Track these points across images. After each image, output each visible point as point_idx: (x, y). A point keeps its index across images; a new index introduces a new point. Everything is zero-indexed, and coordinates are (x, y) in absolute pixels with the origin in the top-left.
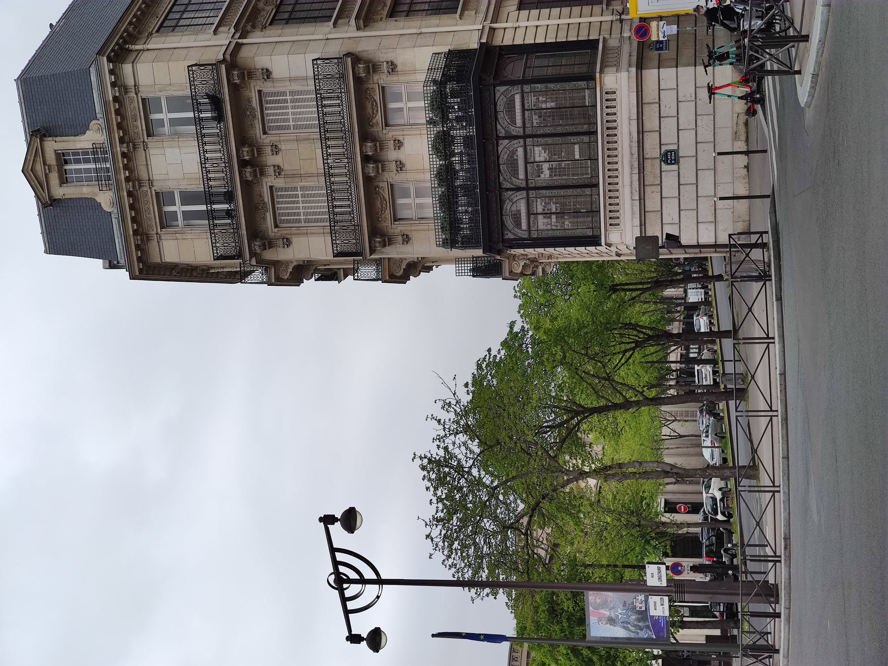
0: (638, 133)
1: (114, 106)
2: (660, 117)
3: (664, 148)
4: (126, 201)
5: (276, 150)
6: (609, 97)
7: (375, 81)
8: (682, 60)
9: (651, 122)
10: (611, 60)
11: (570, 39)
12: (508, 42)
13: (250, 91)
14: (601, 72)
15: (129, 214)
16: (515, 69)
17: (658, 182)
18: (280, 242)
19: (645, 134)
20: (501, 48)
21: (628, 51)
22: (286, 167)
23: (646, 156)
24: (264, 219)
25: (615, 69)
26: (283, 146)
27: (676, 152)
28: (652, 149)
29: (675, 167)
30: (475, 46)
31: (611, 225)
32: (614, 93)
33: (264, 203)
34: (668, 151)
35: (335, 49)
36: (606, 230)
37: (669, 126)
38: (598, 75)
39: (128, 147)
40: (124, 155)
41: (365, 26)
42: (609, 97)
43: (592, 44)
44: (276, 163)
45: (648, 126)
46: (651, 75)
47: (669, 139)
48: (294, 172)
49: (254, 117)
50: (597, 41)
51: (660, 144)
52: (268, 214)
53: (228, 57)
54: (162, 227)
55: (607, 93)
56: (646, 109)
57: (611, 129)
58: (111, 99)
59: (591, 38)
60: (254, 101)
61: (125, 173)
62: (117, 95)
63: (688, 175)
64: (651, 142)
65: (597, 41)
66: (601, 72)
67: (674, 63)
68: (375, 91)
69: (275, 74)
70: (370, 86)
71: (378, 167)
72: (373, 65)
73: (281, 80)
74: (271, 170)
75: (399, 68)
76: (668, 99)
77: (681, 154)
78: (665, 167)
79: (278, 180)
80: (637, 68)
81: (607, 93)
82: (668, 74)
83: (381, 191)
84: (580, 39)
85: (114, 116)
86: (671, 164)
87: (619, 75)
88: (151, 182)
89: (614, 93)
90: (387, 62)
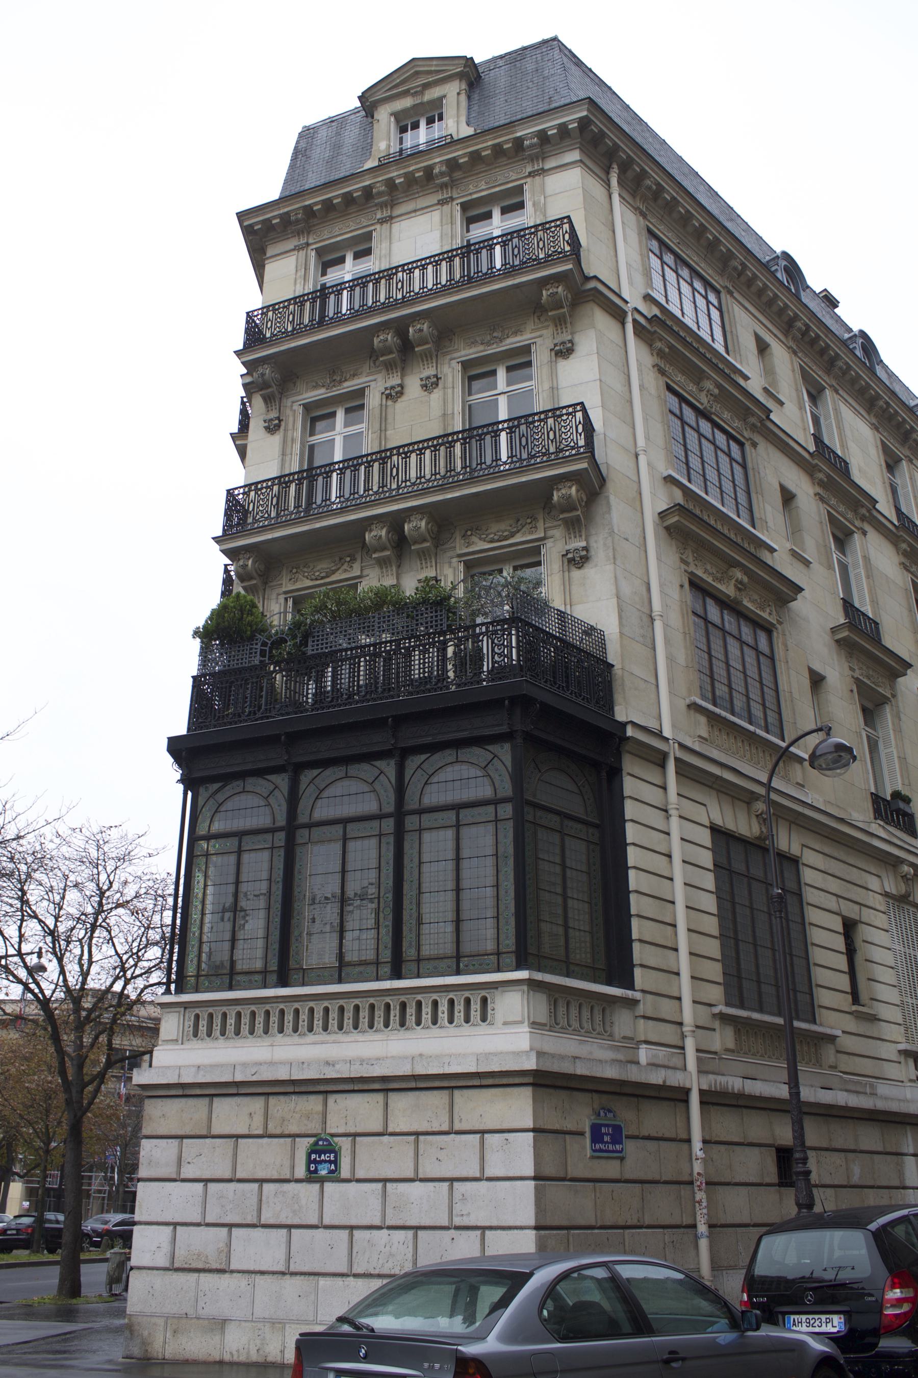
0: (384, 1079)
1: (506, 142)
2: (417, 1134)
3: (344, 1144)
4: (355, 187)
5: (430, 385)
6: (476, 1006)
7: (550, 533)
8: (556, 1191)
9: (408, 1111)
10: (561, 1009)
11: (635, 922)
12: (629, 786)
13: (533, 331)
14: (532, 984)
15: (335, 194)
16: (560, 790)
17: (272, 1129)
18: (273, 415)
19: (380, 1097)
20: (615, 774)
21: (588, 1054)
22: (401, 404)
23: (331, 1099)
24: (316, 387)
25: (543, 1017)
26: (437, 395)
27: (334, 1176)
28: (352, 1113)
29: (301, 1172)
30: (621, 714)
31: (197, 1017)
32: (484, 1019)
33: (341, 382)
34: (336, 1152)
35: (610, 454)
36: (186, 1006)
37: (390, 1158)
38: (523, 974)
39: (442, 174)
40: (428, 170)
41: (837, 641)
42: (476, 1006)
43: (619, 969)
44: (406, 391)
45: (400, 1103)
46: (518, 1108)
47: (374, 1158)
48: (390, 420)
49: (489, 344)
50: (631, 986)
51: (355, 1135)
52: (323, 390)
53: (592, 284)
54: (463, 363)
55: (484, 1001)
56: (438, 1099)
57: (402, 1013)
58: (519, 134)
59: (638, 972)
60: (518, 338)
61: (399, 176)
62: (527, 143)
63: (279, 1203)
64: (360, 1111)
65: (631, 986)
66: (532, 984)
67: (550, 1170)
68: (531, 533)
69: (564, 366)
70: (540, 524)
71: (384, 549)
72: (578, 519)
73: (553, 374)
74: (395, 381)
75: (576, 574)
76: (459, 1156)
77: (328, 1186)
78: (304, 1144)
79: (378, 396)
80: (535, 1073)
81: (484, 1001)
82: (520, 1154)
83: (345, 566)
84: (636, 947)
85: (490, 143)
86: (309, 1161)
87: (525, 1028)
88: (389, 219)
89: (484, 1019)
90: (586, 549)
